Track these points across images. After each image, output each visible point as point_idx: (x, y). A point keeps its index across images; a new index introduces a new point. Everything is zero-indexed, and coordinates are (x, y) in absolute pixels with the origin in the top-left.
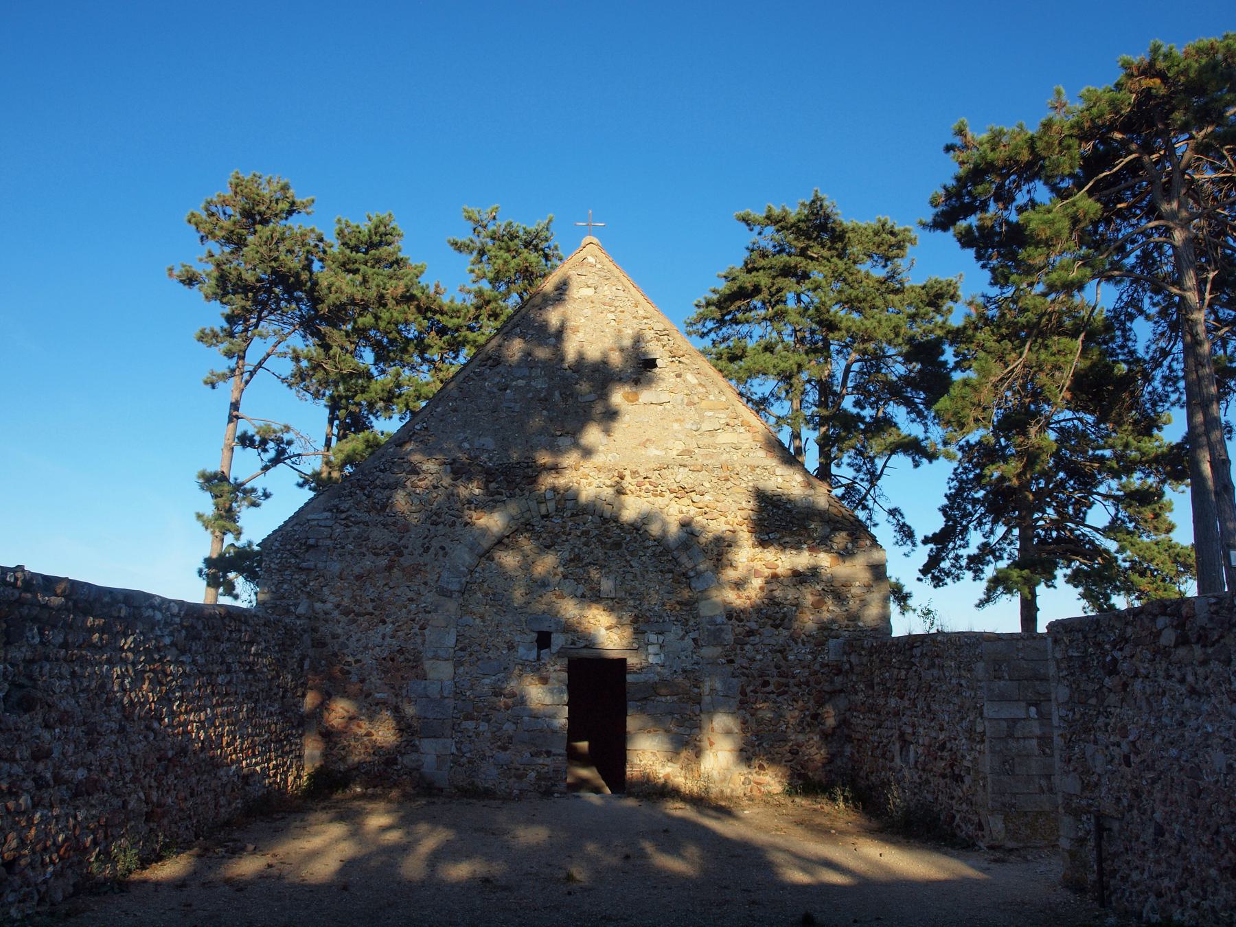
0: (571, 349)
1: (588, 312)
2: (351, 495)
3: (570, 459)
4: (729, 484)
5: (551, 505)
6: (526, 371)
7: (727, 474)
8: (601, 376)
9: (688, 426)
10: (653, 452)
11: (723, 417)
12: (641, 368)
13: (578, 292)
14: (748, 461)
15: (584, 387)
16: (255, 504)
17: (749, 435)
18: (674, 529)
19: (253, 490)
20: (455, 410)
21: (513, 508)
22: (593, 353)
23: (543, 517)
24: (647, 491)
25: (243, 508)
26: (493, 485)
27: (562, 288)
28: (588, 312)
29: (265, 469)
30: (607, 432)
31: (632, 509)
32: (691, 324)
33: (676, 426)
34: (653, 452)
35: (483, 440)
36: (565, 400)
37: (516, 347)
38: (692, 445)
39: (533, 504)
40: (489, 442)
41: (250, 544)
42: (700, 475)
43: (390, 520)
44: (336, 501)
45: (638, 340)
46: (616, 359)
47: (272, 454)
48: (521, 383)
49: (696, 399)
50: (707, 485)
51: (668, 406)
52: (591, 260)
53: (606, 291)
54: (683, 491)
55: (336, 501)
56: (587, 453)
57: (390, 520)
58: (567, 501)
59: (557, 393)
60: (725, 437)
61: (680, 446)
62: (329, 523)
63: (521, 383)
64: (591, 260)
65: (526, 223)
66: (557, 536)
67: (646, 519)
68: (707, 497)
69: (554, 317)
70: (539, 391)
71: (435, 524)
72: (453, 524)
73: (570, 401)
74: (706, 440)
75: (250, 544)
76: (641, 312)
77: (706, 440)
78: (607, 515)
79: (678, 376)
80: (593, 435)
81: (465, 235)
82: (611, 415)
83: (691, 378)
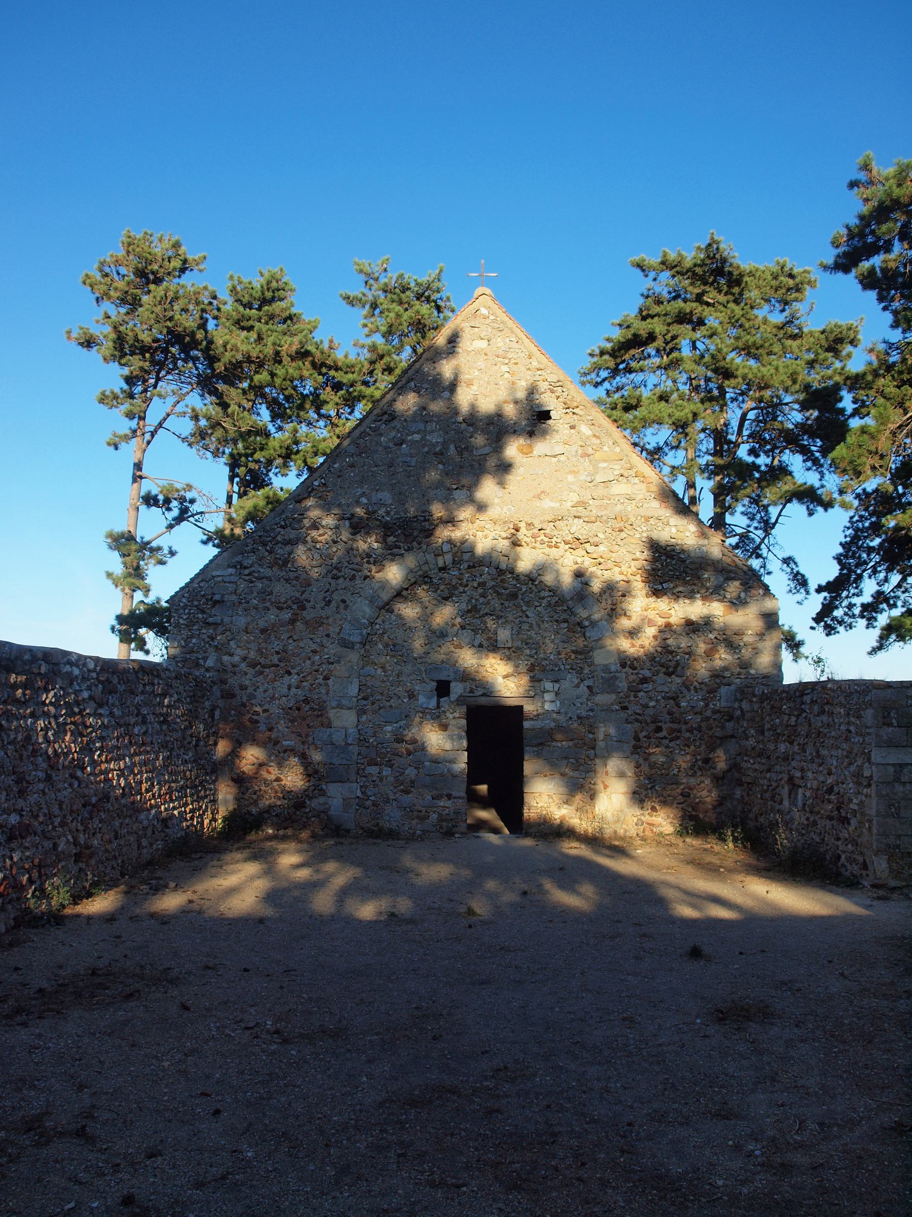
0: (464, 398)
1: (481, 364)
2: (253, 551)
3: (465, 513)
4: (623, 535)
5: (448, 558)
6: (421, 426)
7: (621, 524)
8: (497, 429)
9: (583, 477)
10: (547, 503)
11: (617, 468)
12: (537, 420)
13: (467, 344)
14: (642, 512)
15: (479, 440)
16: (162, 563)
17: (643, 486)
18: (567, 579)
19: (159, 549)
20: (352, 466)
21: (411, 560)
22: (486, 406)
23: (441, 569)
24: (542, 543)
25: (151, 566)
26: (391, 539)
27: (453, 340)
28: (481, 364)
29: (170, 527)
30: (501, 484)
31: (526, 560)
32: (585, 374)
33: (570, 478)
34: (547, 503)
35: (380, 495)
36: (460, 453)
37: (408, 402)
38: (587, 497)
39: (430, 557)
40: (386, 496)
41: (158, 600)
42: (594, 527)
43: (292, 575)
44: (239, 558)
45: (532, 391)
46: (510, 410)
47: (175, 512)
48: (417, 437)
49: (590, 451)
50: (601, 536)
51: (562, 458)
52: (484, 311)
53: (500, 342)
54: (578, 542)
55: (239, 558)
56: (481, 507)
57: (292, 575)
58: (462, 553)
59: (452, 447)
60: (620, 489)
61: (574, 498)
62: (233, 579)
63: (417, 437)
64: (484, 311)
65: (417, 276)
66: (455, 587)
67: (541, 569)
68: (601, 548)
69: (446, 369)
70: (434, 445)
71: (336, 578)
72: (353, 578)
73: (466, 454)
74: (600, 491)
75: (158, 600)
76: (535, 364)
77: (600, 491)
78: (503, 566)
79: (572, 427)
80: (488, 489)
81: (357, 289)
82: (505, 467)
83: (585, 430)
